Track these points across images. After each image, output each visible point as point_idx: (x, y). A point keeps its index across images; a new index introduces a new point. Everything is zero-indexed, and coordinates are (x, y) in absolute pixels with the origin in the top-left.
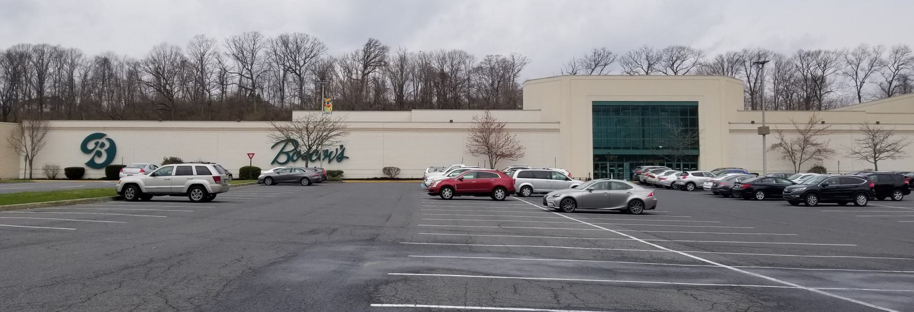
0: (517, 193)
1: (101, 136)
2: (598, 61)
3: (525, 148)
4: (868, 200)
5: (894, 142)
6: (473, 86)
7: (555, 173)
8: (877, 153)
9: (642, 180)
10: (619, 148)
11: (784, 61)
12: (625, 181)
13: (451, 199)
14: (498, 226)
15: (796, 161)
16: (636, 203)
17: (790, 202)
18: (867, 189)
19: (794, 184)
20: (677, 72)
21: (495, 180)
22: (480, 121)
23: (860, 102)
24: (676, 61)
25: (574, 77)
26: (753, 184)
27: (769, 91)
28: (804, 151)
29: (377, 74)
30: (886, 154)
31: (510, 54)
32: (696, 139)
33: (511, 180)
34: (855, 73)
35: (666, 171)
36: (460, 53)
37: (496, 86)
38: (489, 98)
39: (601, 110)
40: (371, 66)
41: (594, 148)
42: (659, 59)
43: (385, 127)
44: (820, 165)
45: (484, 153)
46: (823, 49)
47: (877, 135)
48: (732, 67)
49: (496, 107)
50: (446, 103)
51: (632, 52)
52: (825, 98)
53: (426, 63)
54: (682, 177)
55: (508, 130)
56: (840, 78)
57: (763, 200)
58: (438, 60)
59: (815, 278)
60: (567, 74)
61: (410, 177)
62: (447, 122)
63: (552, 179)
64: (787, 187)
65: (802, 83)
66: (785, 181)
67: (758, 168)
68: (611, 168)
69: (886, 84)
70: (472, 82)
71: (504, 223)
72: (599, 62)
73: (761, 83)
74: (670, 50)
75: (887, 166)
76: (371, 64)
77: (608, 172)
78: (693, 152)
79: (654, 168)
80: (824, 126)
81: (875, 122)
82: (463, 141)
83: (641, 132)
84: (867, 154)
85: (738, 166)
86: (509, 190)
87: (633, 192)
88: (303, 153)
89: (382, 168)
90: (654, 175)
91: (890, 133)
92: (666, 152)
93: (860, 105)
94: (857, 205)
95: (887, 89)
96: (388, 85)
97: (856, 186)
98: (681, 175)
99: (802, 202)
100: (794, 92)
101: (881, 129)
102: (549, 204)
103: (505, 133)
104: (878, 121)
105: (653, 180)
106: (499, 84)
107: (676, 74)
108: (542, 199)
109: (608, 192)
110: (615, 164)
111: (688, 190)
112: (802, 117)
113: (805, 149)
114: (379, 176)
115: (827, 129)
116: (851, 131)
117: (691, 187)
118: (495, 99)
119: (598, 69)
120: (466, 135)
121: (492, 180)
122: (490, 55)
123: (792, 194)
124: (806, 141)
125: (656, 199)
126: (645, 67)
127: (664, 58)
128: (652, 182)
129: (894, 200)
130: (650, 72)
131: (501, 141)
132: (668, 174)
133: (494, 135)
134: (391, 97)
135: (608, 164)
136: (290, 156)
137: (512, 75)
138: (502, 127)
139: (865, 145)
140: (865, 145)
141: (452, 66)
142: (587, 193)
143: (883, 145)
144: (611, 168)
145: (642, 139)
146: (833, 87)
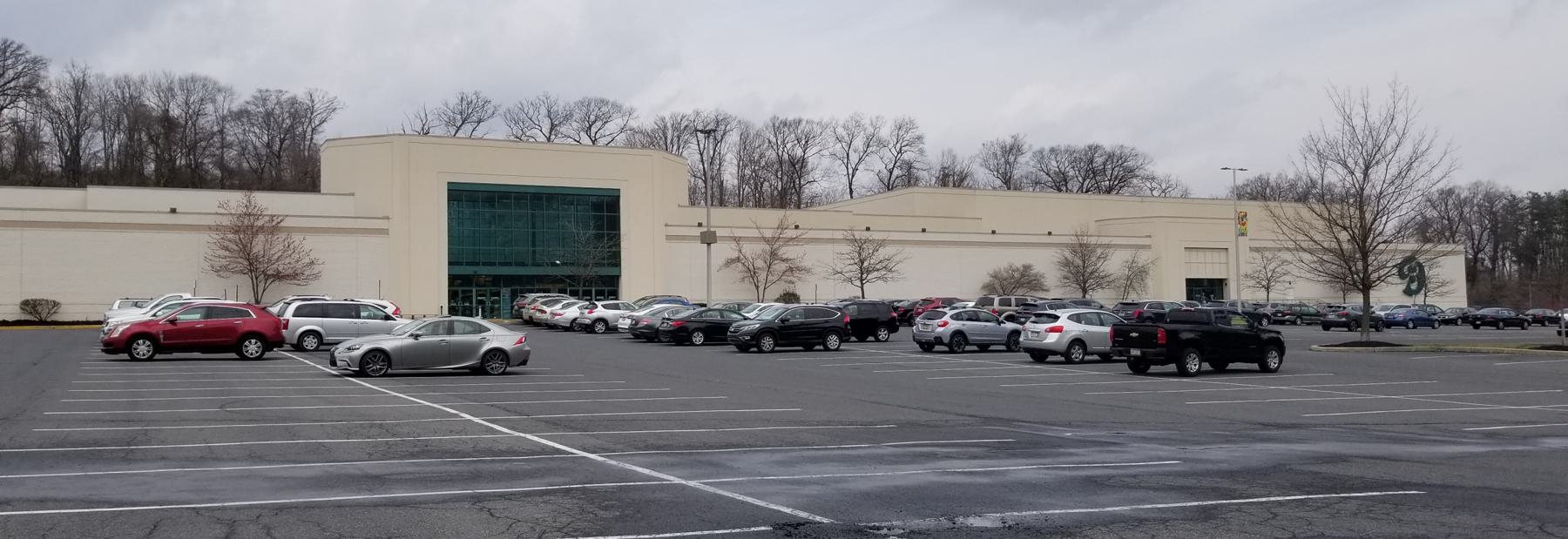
0: (292, 345)
2: (467, 114)
3: (323, 263)
4: (842, 341)
5: (887, 257)
6: (230, 145)
7: (366, 306)
8: (864, 272)
9: (526, 317)
10: (493, 264)
11: (752, 132)
12: (478, 320)
13: (150, 359)
14: (221, 407)
15: (759, 284)
16: (495, 355)
17: (737, 347)
18: (840, 325)
19: (746, 319)
20: (596, 140)
21: (245, 322)
22: (233, 212)
23: (852, 197)
24: (594, 122)
25: (425, 139)
26: (687, 320)
27: (730, 177)
28: (771, 270)
29: (22, 114)
30: (875, 274)
31: (306, 91)
32: (614, 249)
33: (277, 322)
34: (845, 155)
35: (565, 302)
36: (206, 83)
37: (276, 147)
38: (262, 169)
39: (461, 196)
40: (8, 95)
41: (450, 263)
42: (568, 117)
43: (25, 219)
44: (791, 291)
45: (242, 272)
46: (805, 117)
47: (864, 246)
48: (679, 137)
49: (276, 185)
50: (172, 176)
51: (525, 103)
52: (807, 191)
53: (131, 97)
54: (587, 311)
55: (290, 230)
56: (826, 162)
57: (702, 345)
58: (158, 92)
59: (711, 464)
60: (411, 132)
61: (82, 318)
62: (1044, 235)
63: (359, 317)
64: (734, 325)
65: (776, 166)
66: (734, 316)
67: (696, 294)
68: (479, 298)
69: (885, 173)
70: (228, 138)
71: (233, 403)
72: (469, 115)
73: (720, 164)
74: (586, 104)
75: (877, 292)
76: (9, 92)
77: (474, 305)
78: (610, 271)
79: (545, 297)
80: (798, 232)
81: (169, 210)
82: (196, 249)
83: (530, 238)
84: (852, 274)
85: (674, 293)
86: (272, 339)
87: (491, 338)
89: (19, 301)
90: (545, 308)
91: (882, 243)
92: (567, 271)
93: (853, 201)
94: (827, 349)
95: (886, 181)
96: (45, 135)
97: (826, 322)
98: (586, 308)
99: (819, 344)
100: (765, 180)
101: (870, 238)
102: (339, 363)
103: (283, 236)
104: (173, 207)
105: (544, 316)
106: (281, 144)
107: (594, 143)
108: (327, 355)
109: (447, 338)
110: (485, 291)
111: (596, 333)
112: (770, 218)
113: (773, 267)
114: (10, 318)
115: (803, 237)
116: (833, 241)
117: (600, 327)
118: (274, 173)
119: (468, 128)
120: (205, 237)
121: (238, 321)
122: (264, 88)
123: (740, 335)
124: (773, 254)
125: (527, 348)
126: (546, 129)
127: (576, 116)
128: (541, 320)
129: (878, 340)
130: (553, 137)
131: (277, 250)
132: (568, 305)
133: (261, 237)
134: (53, 160)
135: (474, 290)
137: (309, 129)
138: (279, 223)
139: (849, 262)
140: (849, 262)
141: (187, 104)
142: (411, 341)
143: (872, 261)
144: (479, 298)
145: (531, 249)
146: (817, 174)
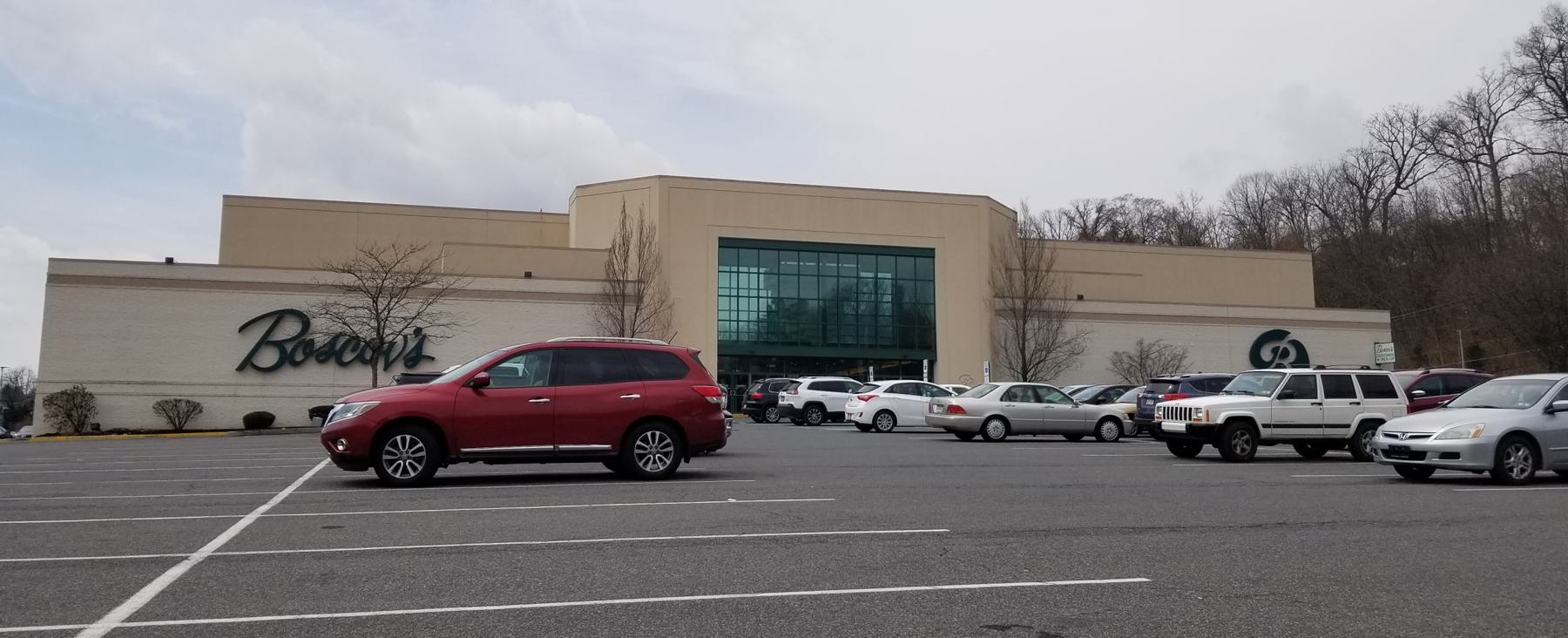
1: (1279, 335)
88: (317, 346)
136: (286, 352)
